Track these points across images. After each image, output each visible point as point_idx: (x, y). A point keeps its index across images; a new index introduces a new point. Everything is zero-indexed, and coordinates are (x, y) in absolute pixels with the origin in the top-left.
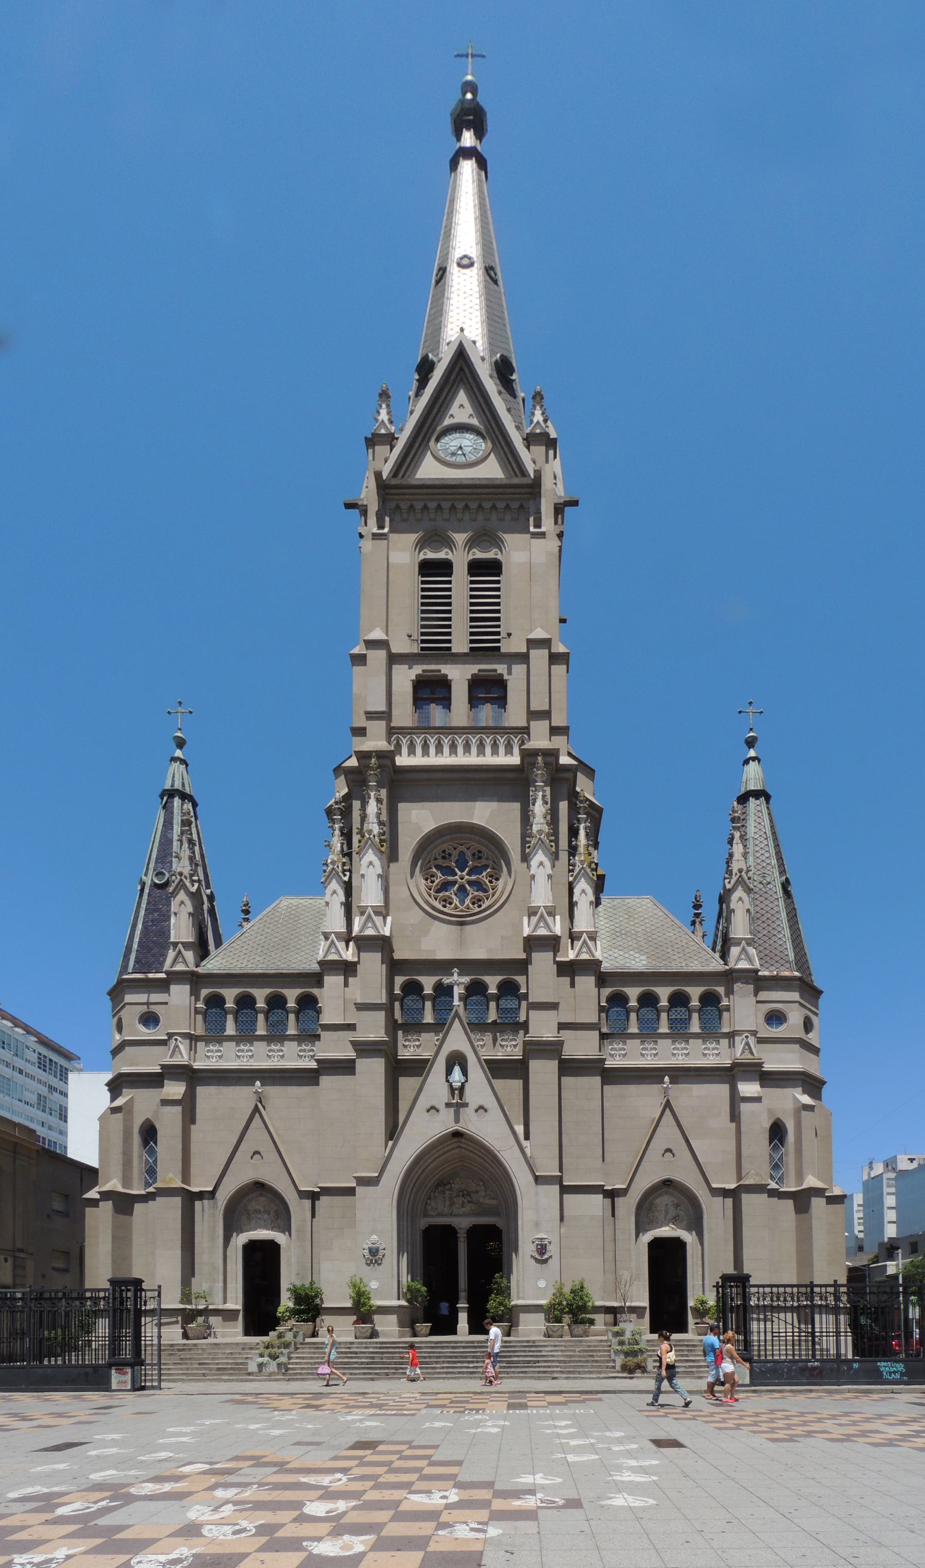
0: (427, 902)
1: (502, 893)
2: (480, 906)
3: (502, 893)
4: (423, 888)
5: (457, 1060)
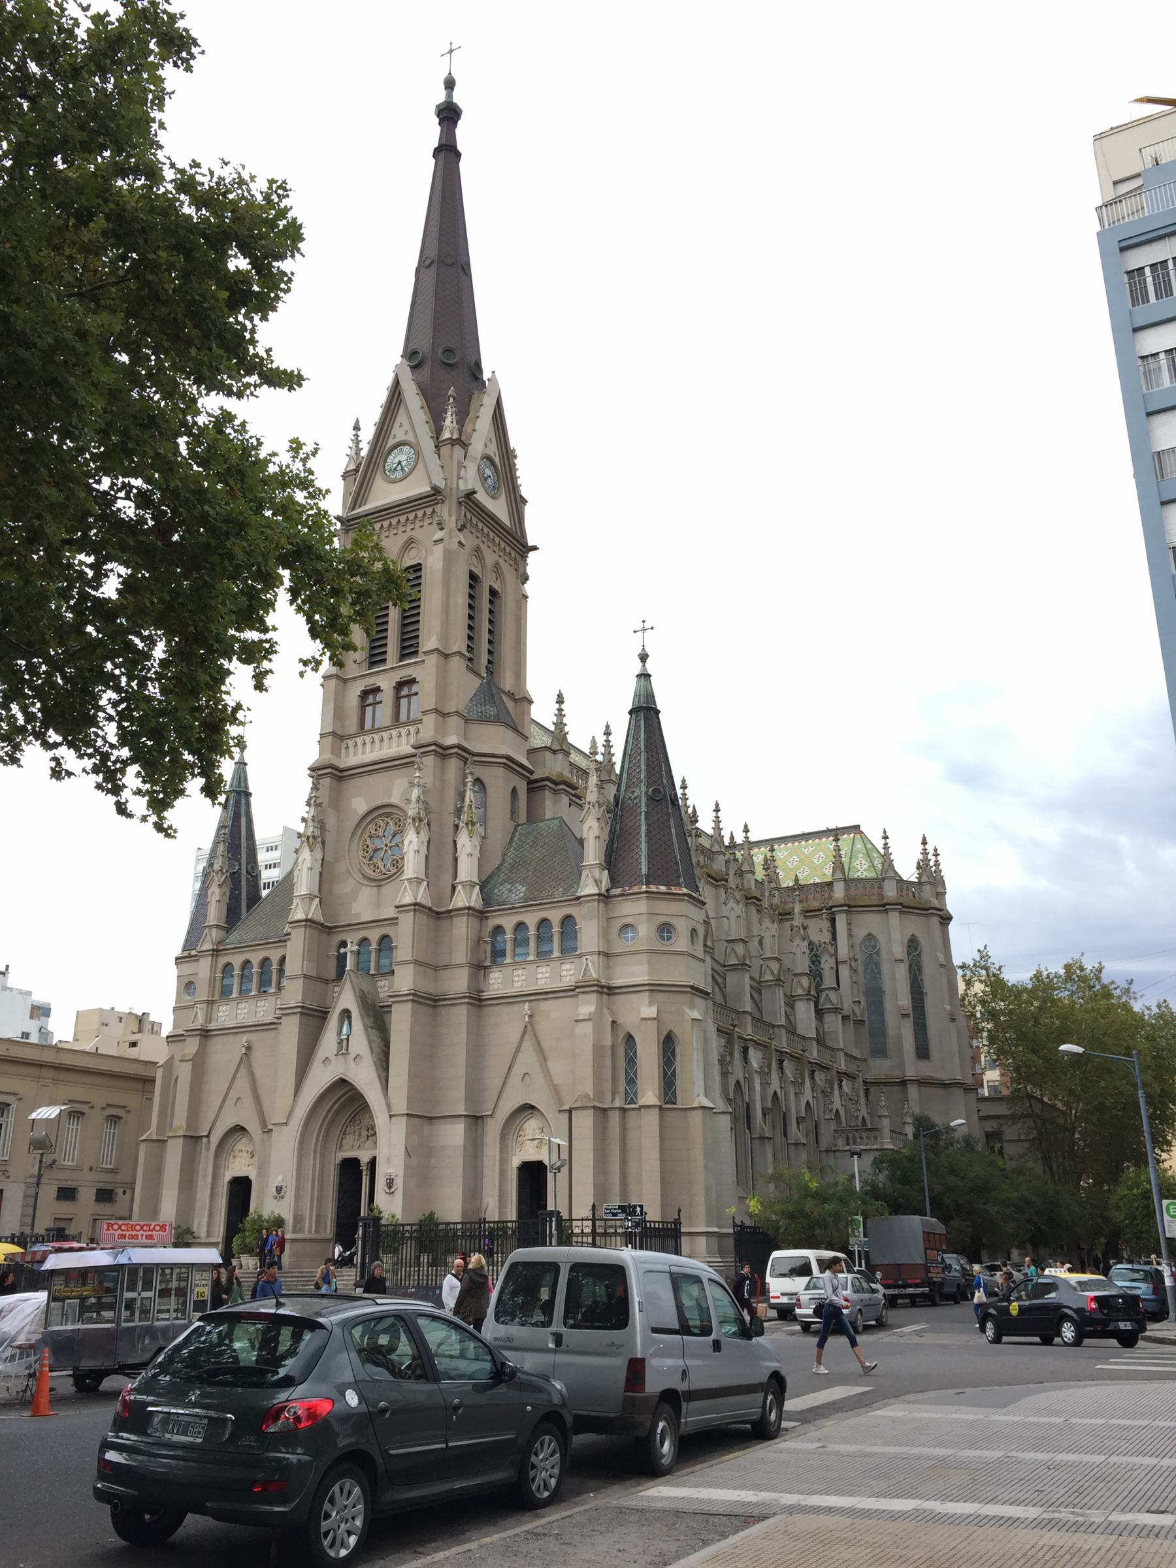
5: (346, 1014)
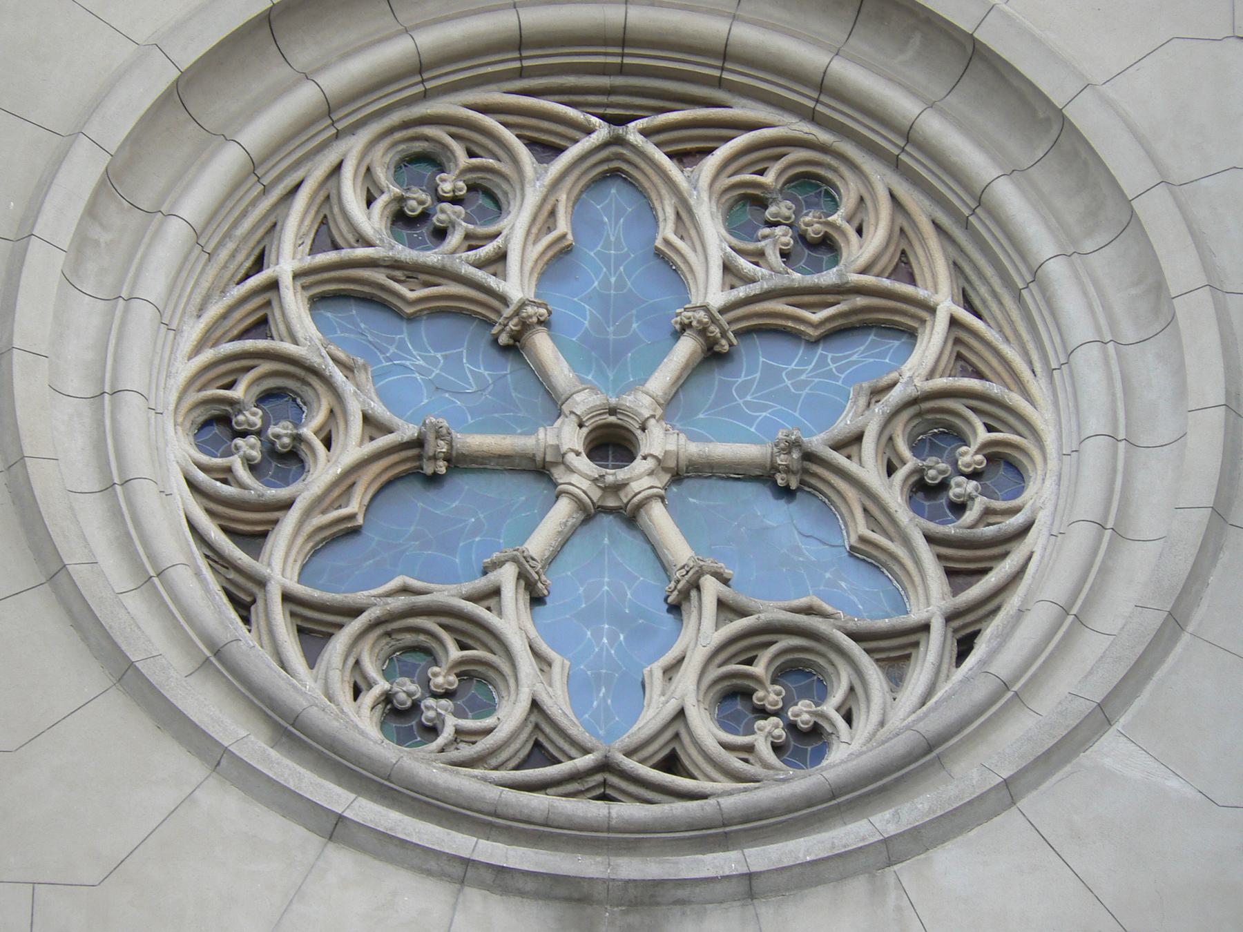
0: (217, 660)
1: (1074, 616)
2: (806, 741)
3: (1074, 616)
4: (170, 515)
